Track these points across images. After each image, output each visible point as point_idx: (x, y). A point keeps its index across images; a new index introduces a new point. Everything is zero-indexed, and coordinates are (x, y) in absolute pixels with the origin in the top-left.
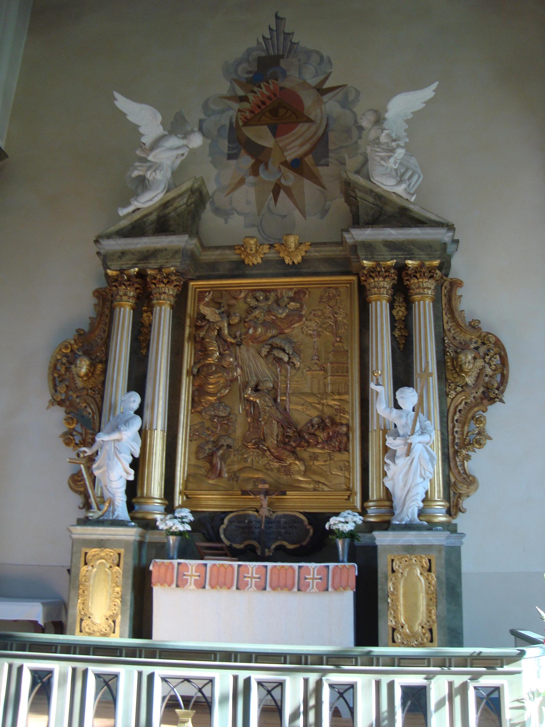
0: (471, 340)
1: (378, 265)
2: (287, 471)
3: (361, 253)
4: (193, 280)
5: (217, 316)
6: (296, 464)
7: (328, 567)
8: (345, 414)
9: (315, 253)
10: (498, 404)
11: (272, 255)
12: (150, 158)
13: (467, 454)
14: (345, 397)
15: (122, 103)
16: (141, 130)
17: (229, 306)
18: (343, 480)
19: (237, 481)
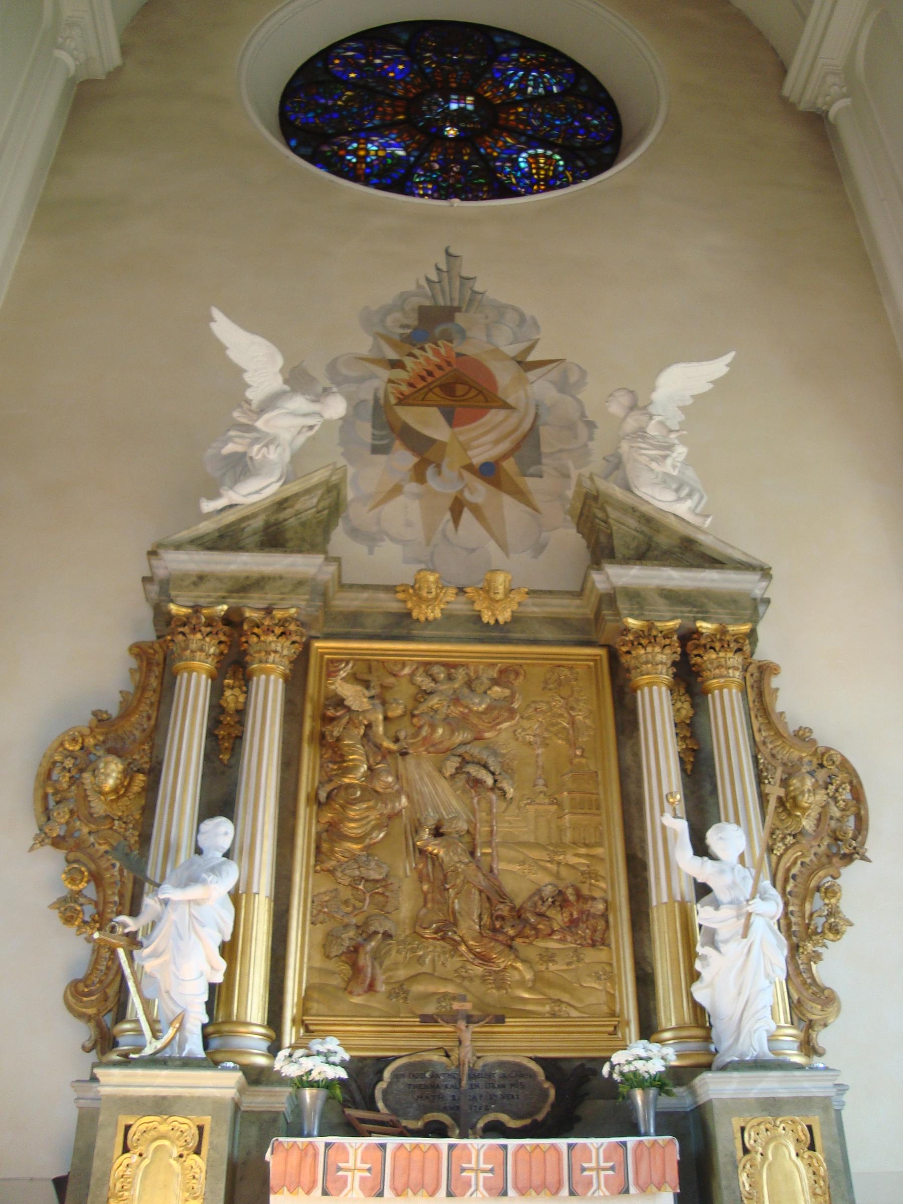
0: (801, 759)
1: (651, 627)
2: (500, 980)
3: (623, 605)
4: (317, 638)
5: (365, 700)
6: (516, 968)
7: (624, 1144)
8: (597, 881)
9: (534, 608)
10: (858, 864)
11: (460, 606)
12: (260, 424)
13: (814, 952)
14: (599, 851)
15: (223, 328)
16: (247, 377)
17: (383, 687)
18: (603, 997)
19: (406, 998)
